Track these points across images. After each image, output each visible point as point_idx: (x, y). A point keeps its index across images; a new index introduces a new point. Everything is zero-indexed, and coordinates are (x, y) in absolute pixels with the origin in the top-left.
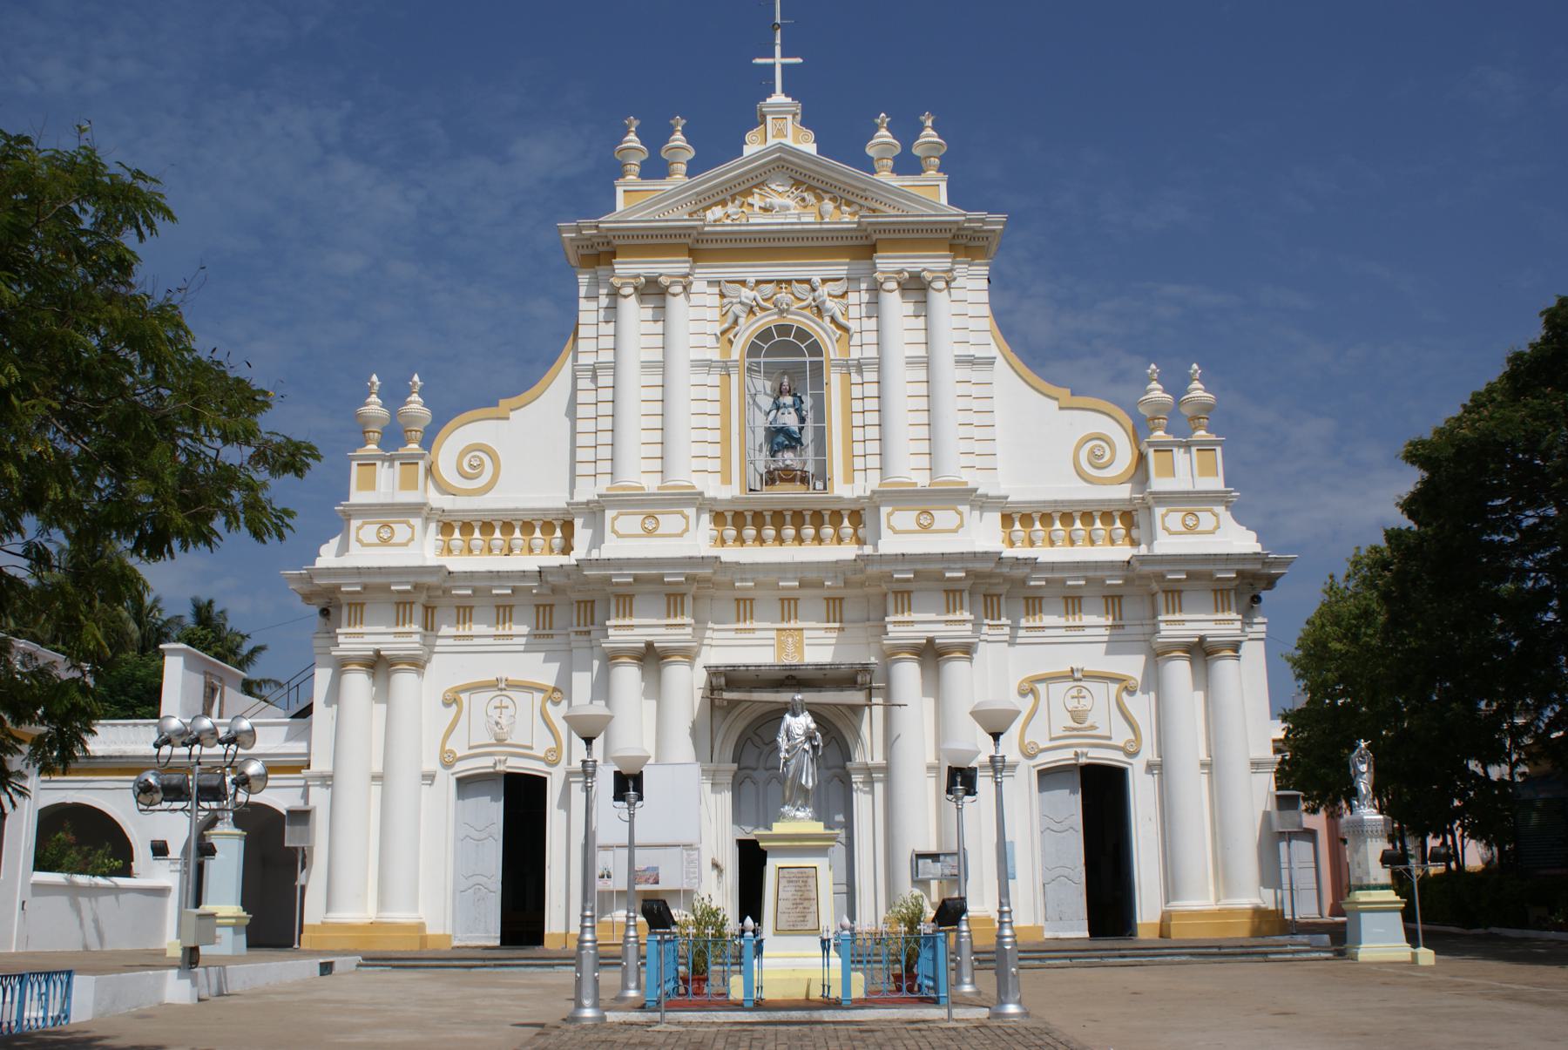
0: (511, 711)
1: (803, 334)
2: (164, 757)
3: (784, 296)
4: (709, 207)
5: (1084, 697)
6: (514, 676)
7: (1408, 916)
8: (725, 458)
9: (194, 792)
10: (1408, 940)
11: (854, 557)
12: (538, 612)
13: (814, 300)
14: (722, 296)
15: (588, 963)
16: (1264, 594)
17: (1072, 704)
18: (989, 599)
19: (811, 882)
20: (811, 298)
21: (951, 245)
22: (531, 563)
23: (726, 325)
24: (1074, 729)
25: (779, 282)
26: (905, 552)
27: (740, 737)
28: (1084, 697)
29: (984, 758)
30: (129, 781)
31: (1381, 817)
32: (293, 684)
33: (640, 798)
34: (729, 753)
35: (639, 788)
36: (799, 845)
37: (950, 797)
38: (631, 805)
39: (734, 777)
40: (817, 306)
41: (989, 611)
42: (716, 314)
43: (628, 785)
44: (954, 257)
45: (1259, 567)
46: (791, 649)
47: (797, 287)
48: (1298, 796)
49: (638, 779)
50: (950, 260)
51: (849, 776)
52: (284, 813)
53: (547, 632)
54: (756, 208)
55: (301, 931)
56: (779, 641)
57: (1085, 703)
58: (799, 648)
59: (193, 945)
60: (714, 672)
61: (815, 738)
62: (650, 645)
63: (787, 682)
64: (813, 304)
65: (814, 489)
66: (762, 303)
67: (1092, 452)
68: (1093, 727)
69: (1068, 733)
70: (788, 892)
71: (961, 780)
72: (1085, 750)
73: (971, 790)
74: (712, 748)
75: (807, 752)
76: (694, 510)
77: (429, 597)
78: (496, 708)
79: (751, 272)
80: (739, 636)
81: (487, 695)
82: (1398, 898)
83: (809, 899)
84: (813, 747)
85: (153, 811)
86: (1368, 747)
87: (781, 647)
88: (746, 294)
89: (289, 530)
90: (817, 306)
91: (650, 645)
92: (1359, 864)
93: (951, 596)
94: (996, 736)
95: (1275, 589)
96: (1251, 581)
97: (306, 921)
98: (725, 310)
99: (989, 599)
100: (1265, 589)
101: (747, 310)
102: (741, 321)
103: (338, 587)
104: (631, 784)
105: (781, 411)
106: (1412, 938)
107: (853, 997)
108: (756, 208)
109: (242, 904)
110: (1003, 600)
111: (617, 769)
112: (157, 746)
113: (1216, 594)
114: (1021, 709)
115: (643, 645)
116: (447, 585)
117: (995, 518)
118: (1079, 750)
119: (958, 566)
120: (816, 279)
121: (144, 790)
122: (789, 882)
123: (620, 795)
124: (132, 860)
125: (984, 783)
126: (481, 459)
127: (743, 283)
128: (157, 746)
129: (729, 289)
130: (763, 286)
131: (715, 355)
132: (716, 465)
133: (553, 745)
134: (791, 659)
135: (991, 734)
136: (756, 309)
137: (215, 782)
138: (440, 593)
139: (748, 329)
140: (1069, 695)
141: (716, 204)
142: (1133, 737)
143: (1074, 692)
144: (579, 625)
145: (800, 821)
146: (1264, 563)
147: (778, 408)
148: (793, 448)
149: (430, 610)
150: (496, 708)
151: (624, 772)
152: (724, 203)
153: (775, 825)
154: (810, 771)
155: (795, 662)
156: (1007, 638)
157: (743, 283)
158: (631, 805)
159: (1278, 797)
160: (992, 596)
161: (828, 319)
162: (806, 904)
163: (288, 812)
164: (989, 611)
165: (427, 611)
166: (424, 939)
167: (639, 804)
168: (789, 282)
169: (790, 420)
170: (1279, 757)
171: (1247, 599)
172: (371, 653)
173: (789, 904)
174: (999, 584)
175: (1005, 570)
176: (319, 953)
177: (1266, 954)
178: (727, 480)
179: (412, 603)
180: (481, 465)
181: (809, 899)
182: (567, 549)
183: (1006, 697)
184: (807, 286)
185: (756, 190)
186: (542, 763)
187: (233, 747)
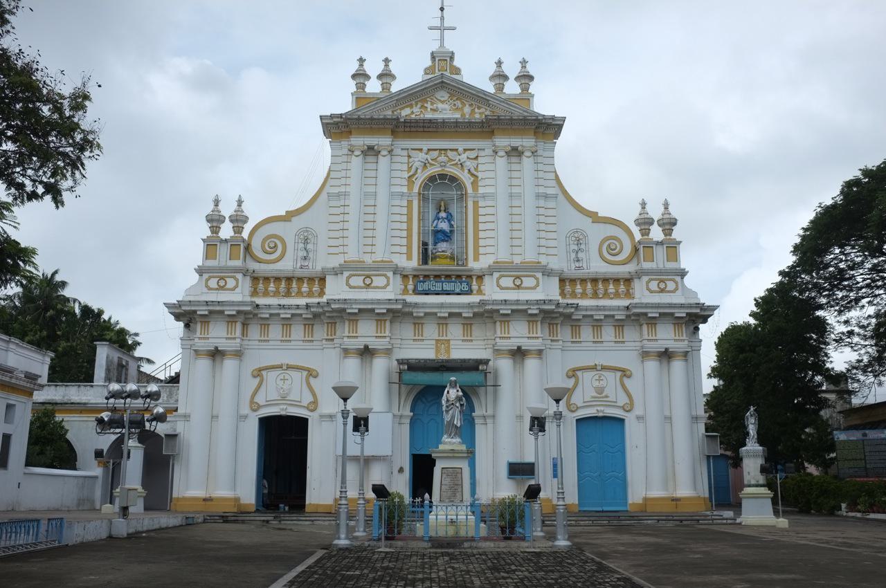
0: (289, 382)
1: (453, 179)
2: (111, 404)
3: (443, 158)
4: (403, 108)
5: (602, 380)
6: (292, 363)
7: (774, 502)
8: (409, 246)
9: (126, 424)
10: (775, 515)
11: (478, 301)
12: (594, 329)
13: (459, 160)
14: (409, 157)
15: (343, 516)
16: (701, 326)
17: (596, 384)
18: (551, 326)
19: (459, 475)
20: (458, 159)
21: (535, 132)
22: (302, 301)
23: (411, 174)
24: (598, 398)
25: (441, 150)
26: (507, 298)
27: (415, 396)
28: (602, 380)
29: (551, 412)
30: (91, 418)
31: (761, 448)
32: (168, 365)
33: (367, 431)
34: (408, 407)
35: (366, 425)
36: (453, 455)
37: (531, 433)
38: (363, 434)
39: (411, 420)
40: (461, 164)
41: (650, 333)
42: (405, 167)
43: (361, 423)
44: (537, 138)
45: (554, 307)
46: (443, 351)
47: (450, 153)
48: (717, 436)
49: (366, 420)
50: (534, 140)
51: (473, 420)
52: (163, 436)
53: (469, 338)
54: (429, 110)
55: (171, 502)
56: (437, 346)
57: (603, 383)
58: (448, 351)
59: (125, 506)
60: (400, 362)
61: (462, 400)
62: (519, 348)
63: (441, 369)
64: (459, 163)
65: (457, 264)
66: (430, 161)
67: (609, 245)
68: (607, 397)
69: (267, 403)
70: (447, 481)
71: (538, 424)
72: (602, 408)
73: (542, 429)
74: (399, 404)
75: (457, 407)
76: (392, 273)
77: (246, 318)
78: (281, 380)
79: (425, 144)
80: (283, 344)
81: (278, 372)
82: (770, 492)
83: (458, 485)
84: (462, 405)
85: (106, 433)
86: (755, 410)
87: (438, 350)
88: (422, 156)
89: (57, 275)
90: (461, 164)
91: (519, 348)
92: (749, 473)
93: (379, 323)
94: (345, 400)
95: (707, 323)
96: (694, 318)
97: (174, 496)
98: (410, 165)
99: (551, 326)
100: (702, 323)
101: (423, 164)
102: (419, 171)
103: (195, 312)
104: (362, 422)
105: (440, 221)
106: (776, 513)
107: (481, 535)
108: (429, 110)
109: (142, 486)
110: (559, 326)
111: (355, 415)
112: (107, 398)
113: (529, 324)
114: (358, 386)
115: (362, 347)
116: (256, 312)
117: (555, 281)
118: (599, 409)
119: (535, 307)
120: (461, 149)
121: (100, 421)
122: (447, 475)
123: (356, 429)
124: (76, 461)
125: (550, 426)
126: (276, 244)
127: (421, 150)
128: (107, 398)
129: (413, 153)
130: (431, 152)
131: (405, 190)
132: (404, 250)
133: (312, 400)
134: (443, 357)
135: (555, 400)
136: (428, 165)
137: (139, 418)
138: (251, 316)
139: (422, 177)
140: (278, 379)
141: (407, 107)
142: (628, 402)
143: (597, 377)
144: (201, 334)
145: (450, 442)
146: (701, 309)
147: (439, 219)
148: (447, 241)
149: (245, 326)
150: (281, 380)
151: (359, 416)
152: (411, 106)
153: (440, 446)
154: (459, 417)
155: (445, 358)
156: (560, 347)
157: (421, 150)
158: (363, 434)
159: (707, 436)
160: (553, 324)
161: (466, 171)
162: (456, 487)
163: (166, 435)
164: (650, 333)
165: (244, 327)
166: (240, 505)
167: (366, 433)
168: (446, 150)
169: (444, 226)
170: (708, 415)
171: (692, 328)
172: (213, 349)
173: (447, 487)
174: (556, 318)
175: (561, 310)
176: (182, 512)
177: (698, 520)
178: (409, 258)
179: (236, 322)
180: (276, 246)
181: (458, 485)
182: (322, 293)
183: (560, 382)
184: (455, 153)
185: (428, 99)
186: (306, 410)
187: (148, 400)
